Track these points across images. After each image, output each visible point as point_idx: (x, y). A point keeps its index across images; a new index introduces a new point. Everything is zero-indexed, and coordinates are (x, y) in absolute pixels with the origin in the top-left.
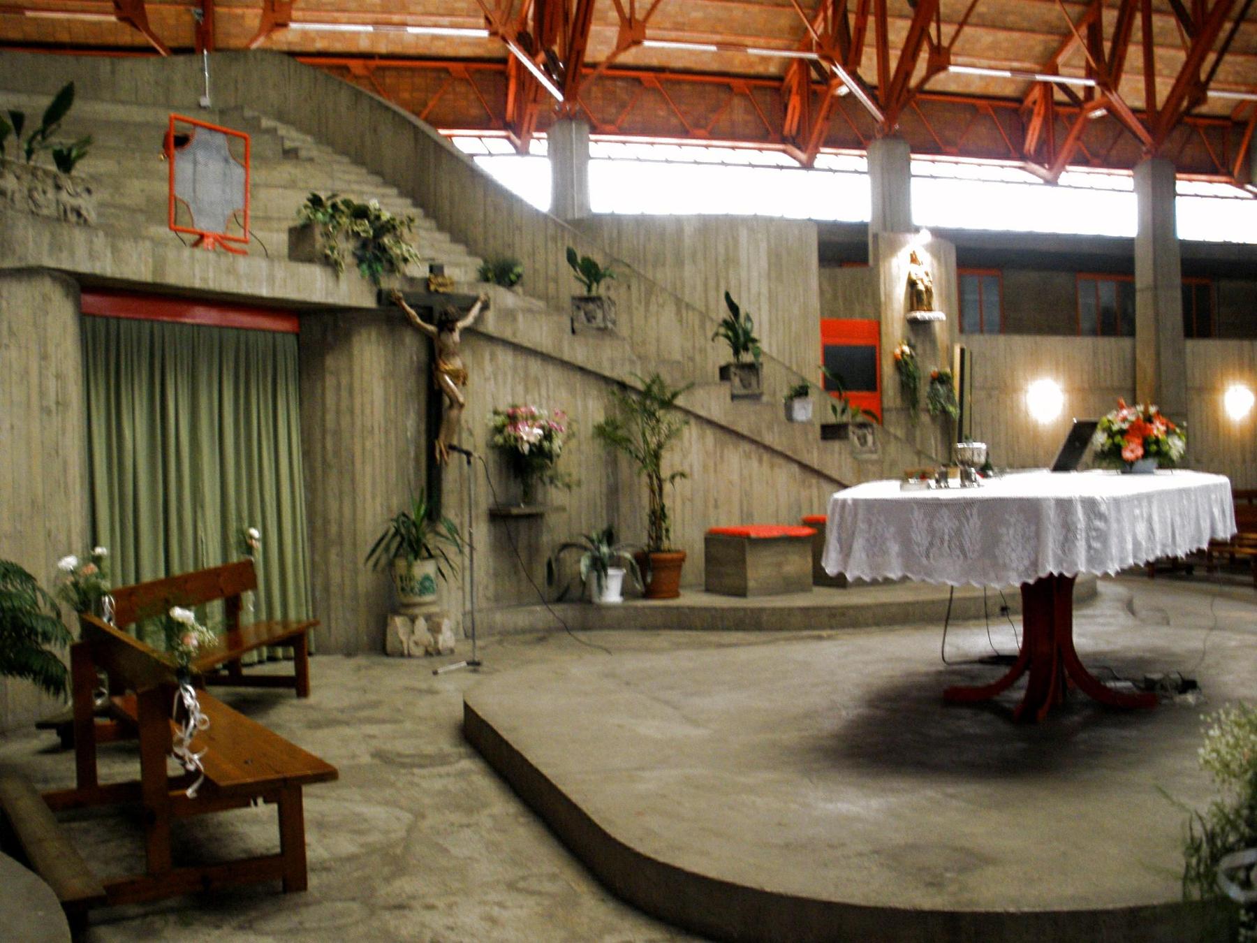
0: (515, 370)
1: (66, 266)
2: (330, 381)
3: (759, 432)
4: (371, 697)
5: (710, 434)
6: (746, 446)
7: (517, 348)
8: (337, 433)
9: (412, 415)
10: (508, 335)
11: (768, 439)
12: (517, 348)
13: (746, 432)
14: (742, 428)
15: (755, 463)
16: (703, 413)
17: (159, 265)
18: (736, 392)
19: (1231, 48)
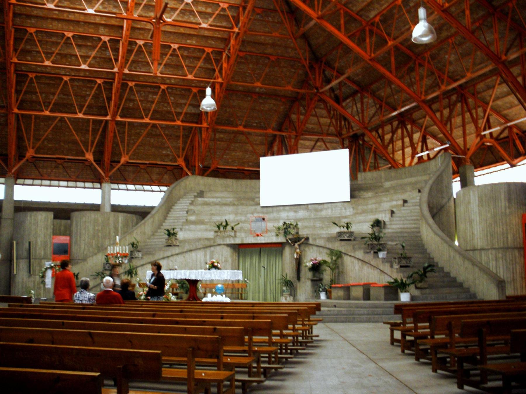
4: (408, 265)
5: (360, 262)
6: (368, 265)
7: (317, 246)
11: (372, 263)
12: (317, 246)
14: (366, 260)
15: (370, 269)
17: (242, 240)
19: (405, 146)
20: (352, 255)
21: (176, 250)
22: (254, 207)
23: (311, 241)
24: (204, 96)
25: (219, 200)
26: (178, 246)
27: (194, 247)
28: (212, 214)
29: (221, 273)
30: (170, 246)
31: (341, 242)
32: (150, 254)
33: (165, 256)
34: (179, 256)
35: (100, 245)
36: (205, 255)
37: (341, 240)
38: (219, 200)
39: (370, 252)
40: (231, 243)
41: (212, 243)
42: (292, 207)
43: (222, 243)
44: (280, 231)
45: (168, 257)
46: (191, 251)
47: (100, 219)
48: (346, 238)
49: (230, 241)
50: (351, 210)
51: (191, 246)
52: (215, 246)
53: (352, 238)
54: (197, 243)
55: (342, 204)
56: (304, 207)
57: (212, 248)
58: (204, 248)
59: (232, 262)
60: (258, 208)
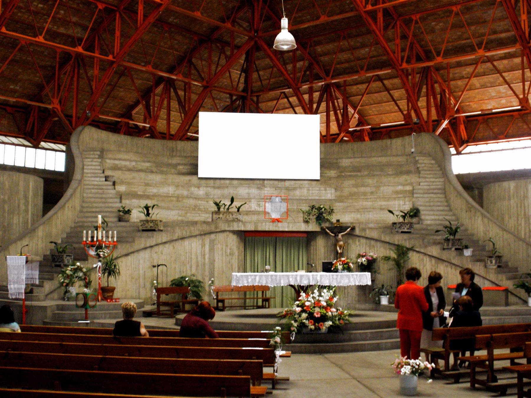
0: (366, 244)
1: (232, 229)
2: (312, 248)
3: (450, 259)
5: (433, 261)
6: (447, 264)
7: (367, 238)
8: (313, 259)
9: (332, 255)
10: (363, 235)
11: (453, 261)
12: (367, 238)
13: (445, 259)
14: (444, 258)
15: (449, 269)
16: (430, 254)
18: (445, 247)
20: (422, 251)
21: (163, 237)
22: (188, 178)
23: (357, 232)
24: (278, 29)
25: (134, 164)
26: (162, 231)
27: (188, 234)
28: (147, 185)
29: (337, 275)
30: (154, 230)
31: (402, 234)
32: (127, 242)
33: (148, 245)
34: (167, 245)
35: (6, 224)
36: (203, 245)
37: (402, 232)
38: (134, 164)
39: (451, 249)
40: (240, 229)
41: (213, 228)
42: (242, 182)
43: (227, 229)
44: (311, 217)
45: (151, 247)
46: (183, 238)
47: (7, 183)
48: (406, 230)
49: (238, 227)
50: (333, 191)
51: (184, 232)
52: (217, 232)
53: (412, 230)
54: (192, 228)
55: (310, 182)
56: (258, 182)
57: (213, 236)
58: (201, 235)
59: (239, 256)
60: (194, 179)
